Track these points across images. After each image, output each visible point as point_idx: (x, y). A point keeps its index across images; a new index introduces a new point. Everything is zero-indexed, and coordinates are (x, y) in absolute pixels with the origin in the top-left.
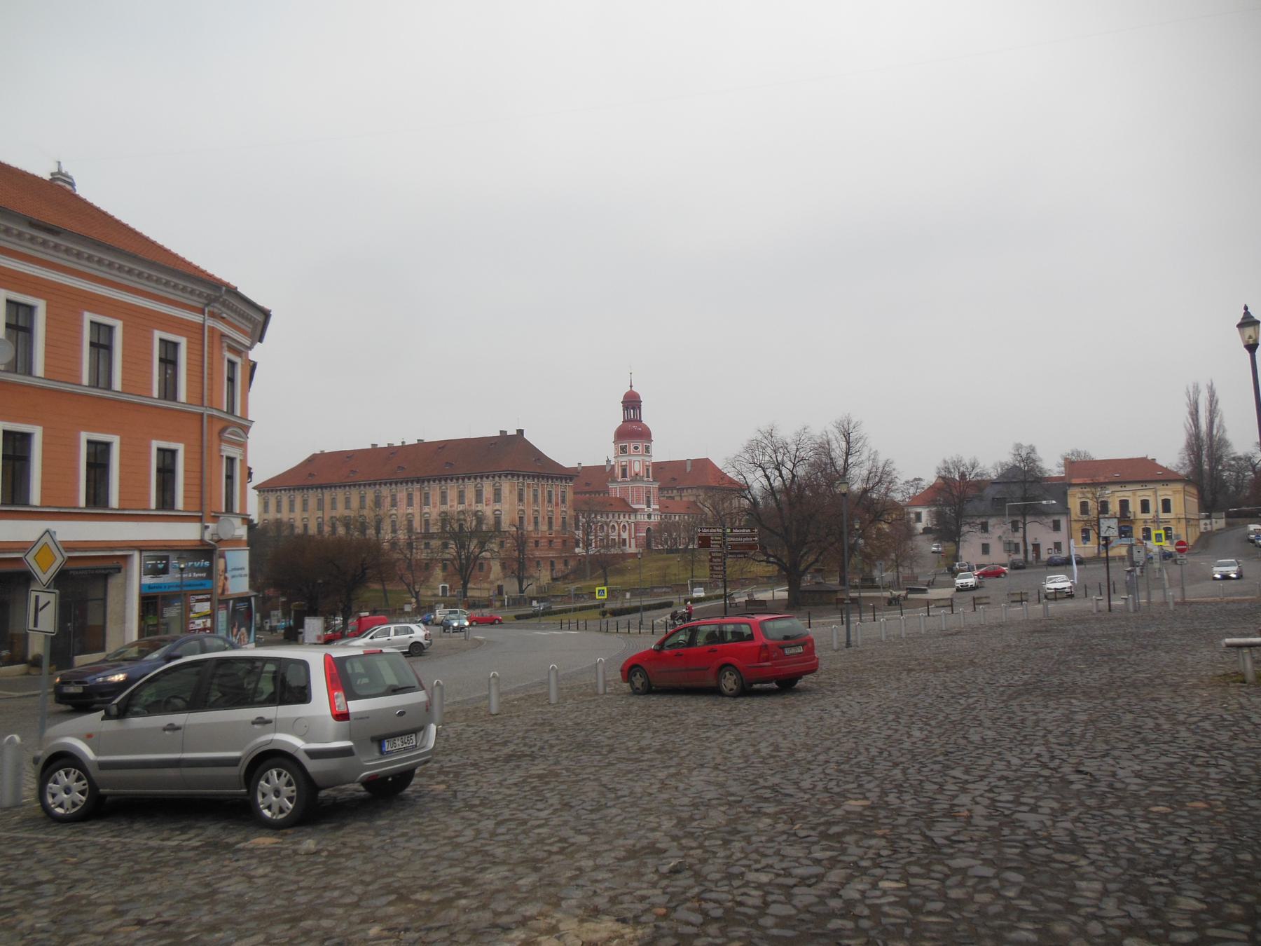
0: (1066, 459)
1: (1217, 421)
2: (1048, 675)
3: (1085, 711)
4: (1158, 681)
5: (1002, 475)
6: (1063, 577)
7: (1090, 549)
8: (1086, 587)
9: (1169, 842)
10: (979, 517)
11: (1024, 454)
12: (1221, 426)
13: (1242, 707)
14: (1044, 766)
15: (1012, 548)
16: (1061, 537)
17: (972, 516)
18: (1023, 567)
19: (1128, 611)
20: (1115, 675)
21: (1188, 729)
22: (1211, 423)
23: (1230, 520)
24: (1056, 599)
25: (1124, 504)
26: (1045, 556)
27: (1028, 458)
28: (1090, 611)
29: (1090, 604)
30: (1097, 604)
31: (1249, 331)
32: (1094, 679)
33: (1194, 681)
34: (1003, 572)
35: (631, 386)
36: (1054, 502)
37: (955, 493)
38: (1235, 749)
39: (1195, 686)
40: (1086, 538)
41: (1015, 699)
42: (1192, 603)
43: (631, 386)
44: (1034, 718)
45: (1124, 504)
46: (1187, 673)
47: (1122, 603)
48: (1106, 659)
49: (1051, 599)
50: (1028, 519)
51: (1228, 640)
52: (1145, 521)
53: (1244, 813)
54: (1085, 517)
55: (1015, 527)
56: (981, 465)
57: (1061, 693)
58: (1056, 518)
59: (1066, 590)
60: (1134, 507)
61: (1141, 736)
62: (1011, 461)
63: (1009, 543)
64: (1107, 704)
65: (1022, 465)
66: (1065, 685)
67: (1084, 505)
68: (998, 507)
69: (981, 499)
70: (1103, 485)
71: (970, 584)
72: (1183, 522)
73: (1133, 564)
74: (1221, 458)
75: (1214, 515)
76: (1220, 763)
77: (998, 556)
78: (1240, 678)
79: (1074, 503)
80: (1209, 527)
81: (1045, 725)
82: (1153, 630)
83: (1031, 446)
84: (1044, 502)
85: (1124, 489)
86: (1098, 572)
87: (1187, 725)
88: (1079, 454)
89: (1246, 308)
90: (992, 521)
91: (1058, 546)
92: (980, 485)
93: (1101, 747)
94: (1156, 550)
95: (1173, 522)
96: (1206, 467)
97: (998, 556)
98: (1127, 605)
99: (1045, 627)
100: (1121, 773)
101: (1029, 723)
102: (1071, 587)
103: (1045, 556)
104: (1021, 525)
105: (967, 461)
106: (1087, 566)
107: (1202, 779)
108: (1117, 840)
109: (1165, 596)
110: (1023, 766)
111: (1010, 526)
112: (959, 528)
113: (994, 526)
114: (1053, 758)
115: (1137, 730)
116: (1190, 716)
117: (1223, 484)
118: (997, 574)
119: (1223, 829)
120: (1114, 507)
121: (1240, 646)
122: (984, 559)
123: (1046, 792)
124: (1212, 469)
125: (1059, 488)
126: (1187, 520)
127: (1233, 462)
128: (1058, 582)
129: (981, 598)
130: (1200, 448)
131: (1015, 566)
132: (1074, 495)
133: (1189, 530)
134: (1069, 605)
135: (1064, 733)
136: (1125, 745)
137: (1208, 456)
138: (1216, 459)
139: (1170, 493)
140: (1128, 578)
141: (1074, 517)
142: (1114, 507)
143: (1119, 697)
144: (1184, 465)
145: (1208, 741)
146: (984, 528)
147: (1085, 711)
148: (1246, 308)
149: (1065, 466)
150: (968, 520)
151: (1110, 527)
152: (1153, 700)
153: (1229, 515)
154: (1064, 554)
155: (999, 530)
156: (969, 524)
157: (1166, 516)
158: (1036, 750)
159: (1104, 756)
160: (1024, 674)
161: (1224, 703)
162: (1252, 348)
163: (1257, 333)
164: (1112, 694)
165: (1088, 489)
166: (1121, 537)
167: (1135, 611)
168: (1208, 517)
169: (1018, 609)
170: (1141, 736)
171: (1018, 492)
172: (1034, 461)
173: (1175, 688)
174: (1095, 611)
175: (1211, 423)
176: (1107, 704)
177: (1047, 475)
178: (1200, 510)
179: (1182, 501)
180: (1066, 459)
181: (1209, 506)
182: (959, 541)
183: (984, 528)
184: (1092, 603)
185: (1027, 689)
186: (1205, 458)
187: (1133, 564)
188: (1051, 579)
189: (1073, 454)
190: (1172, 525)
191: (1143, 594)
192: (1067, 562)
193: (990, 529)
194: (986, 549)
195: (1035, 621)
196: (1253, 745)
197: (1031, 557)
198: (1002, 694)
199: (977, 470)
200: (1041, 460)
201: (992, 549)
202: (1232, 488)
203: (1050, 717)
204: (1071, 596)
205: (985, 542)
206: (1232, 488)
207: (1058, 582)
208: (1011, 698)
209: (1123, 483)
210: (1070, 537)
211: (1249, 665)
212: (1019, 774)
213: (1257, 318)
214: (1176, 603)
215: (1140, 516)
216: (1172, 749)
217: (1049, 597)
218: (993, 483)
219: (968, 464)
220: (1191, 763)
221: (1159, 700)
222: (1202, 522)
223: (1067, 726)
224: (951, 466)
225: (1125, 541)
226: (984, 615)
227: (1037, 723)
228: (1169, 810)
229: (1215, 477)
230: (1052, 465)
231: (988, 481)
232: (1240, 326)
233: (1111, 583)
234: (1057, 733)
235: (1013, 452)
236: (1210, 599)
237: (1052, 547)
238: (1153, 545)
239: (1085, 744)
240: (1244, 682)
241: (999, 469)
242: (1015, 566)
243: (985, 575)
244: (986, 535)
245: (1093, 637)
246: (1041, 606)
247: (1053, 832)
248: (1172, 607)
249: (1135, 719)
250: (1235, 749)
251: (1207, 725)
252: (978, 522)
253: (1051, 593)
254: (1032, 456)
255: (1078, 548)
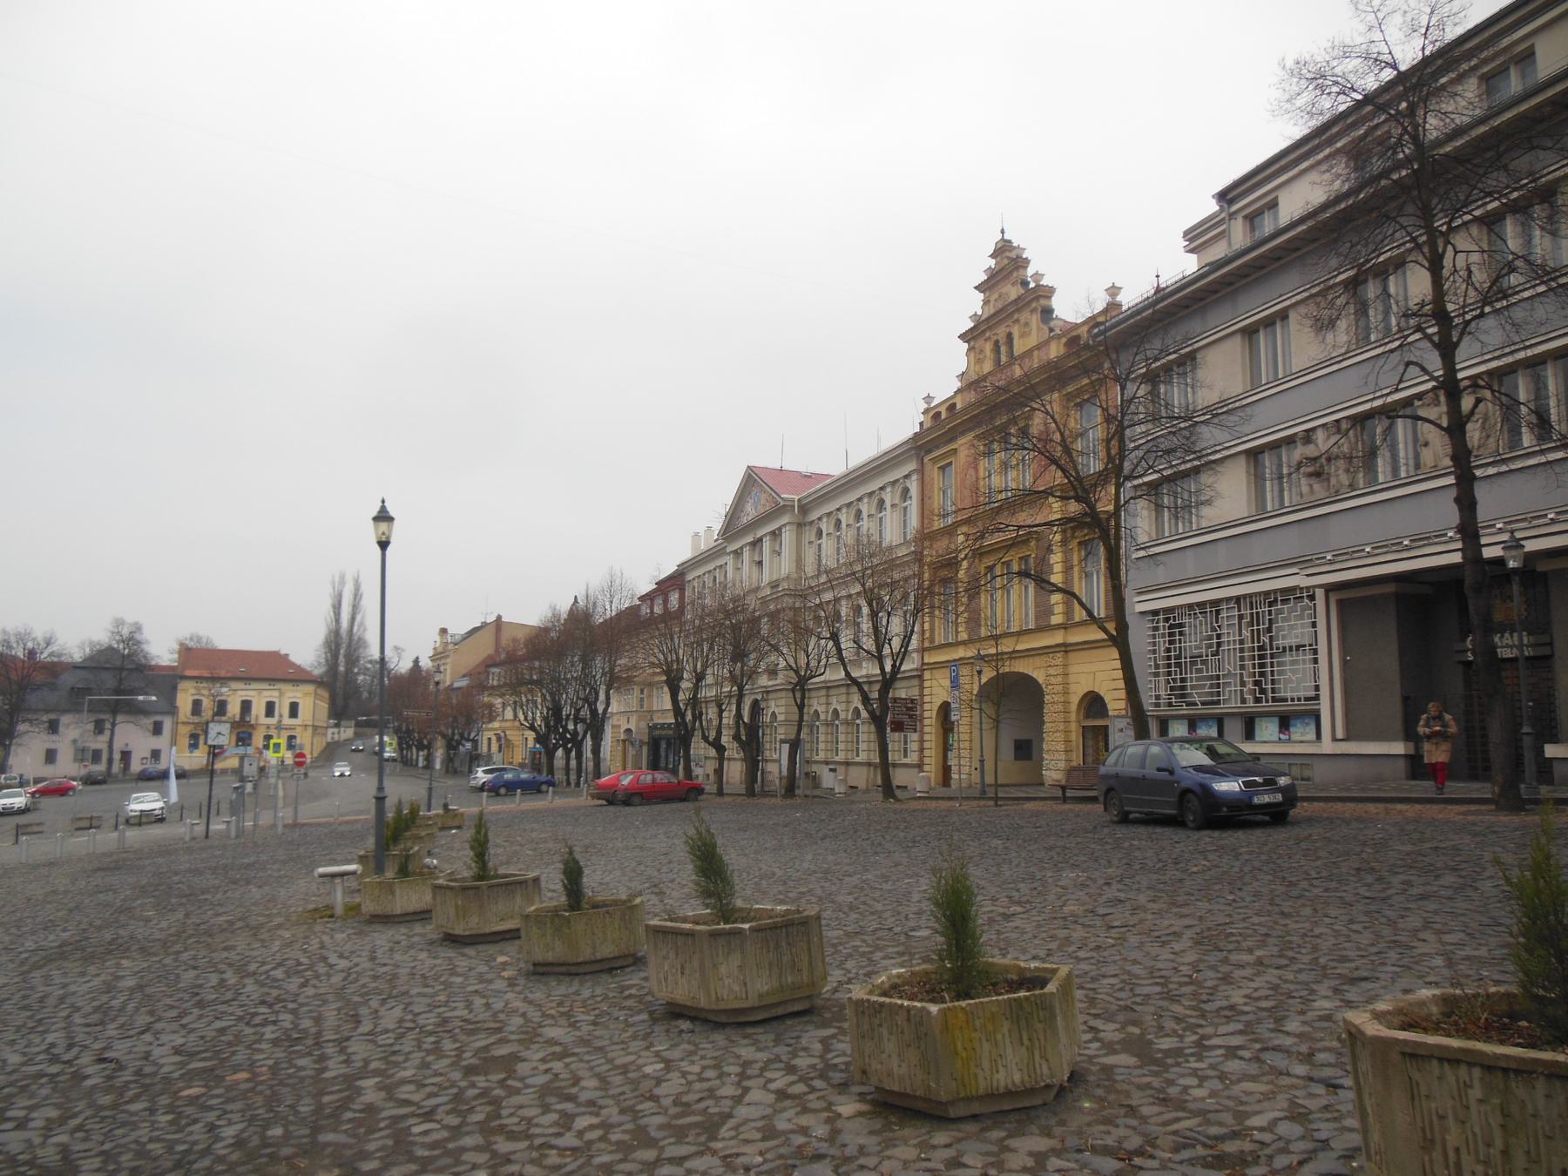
0: (182, 644)
1: (358, 618)
2: (99, 928)
3: (136, 974)
4: (240, 924)
5: (91, 658)
6: (155, 795)
7: (199, 758)
8: (182, 808)
9: (191, 1133)
10: (47, 711)
11: (125, 632)
12: (362, 624)
13: (322, 947)
14: (55, 1059)
15: (81, 754)
16: (161, 742)
17: (36, 711)
18: (102, 782)
19: (228, 837)
20: (189, 922)
21: (257, 982)
22: (353, 619)
23: (360, 730)
24: (140, 824)
25: (246, 706)
26: (136, 766)
27: (131, 639)
28: (182, 839)
29: (183, 830)
30: (192, 830)
31: (383, 526)
32: (161, 930)
33: (279, 920)
34: (72, 788)
35: (1003, 232)
36: (154, 698)
37: (13, 676)
38: (301, 1000)
39: (279, 926)
40: (194, 746)
41: (40, 967)
42: (304, 825)
43: (1003, 232)
44: (61, 992)
45: (246, 706)
46: (275, 911)
47: (223, 827)
48: (184, 900)
49: (134, 825)
50: (120, 718)
51: (321, 870)
52: (268, 727)
53: (290, 1076)
54: (196, 719)
55: (99, 728)
56: (61, 641)
57: (110, 952)
58: (158, 718)
59: (157, 812)
60: (258, 709)
61: (198, 998)
62: (107, 640)
63: (83, 750)
64: (168, 961)
65: (121, 646)
66: (120, 941)
67: (197, 705)
68: (77, 699)
69: (53, 687)
70: (224, 680)
71: (17, 806)
72: (310, 730)
73: (243, 779)
74: (358, 659)
75: (343, 723)
76: (281, 1018)
77: (67, 768)
78: (329, 913)
79: (184, 701)
80: (336, 737)
81: (73, 1000)
82: (252, 859)
83: (136, 623)
84: (141, 698)
85: (248, 687)
86: (199, 787)
87: (257, 977)
88: (199, 639)
89: (383, 502)
90: (65, 719)
91: (156, 754)
92: (55, 669)
93: (142, 1020)
94: (274, 762)
95: (299, 730)
96: (342, 669)
97: (67, 768)
98: (228, 830)
99: (114, 864)
100: (157, 1052)
101: (51, 1001)
102: (162, 808)
103: (136, 766)
104: (108, 725)
105: (39, 633)
106: (191, 781)
107: (255, 1042)
108: (125, 1145)
109: (275, 816)
110: (24, 1064)
111: (91, 727)
112: (12, 725)
113: (69, 725)
114: (70, 1047)
115: (196, 990)
116: (263, 963)
117: (357, 689)
118: (62, 791)
119: (259, 1100)
120: (234, 709)
121: (333, 876)
122: (48, 771)
123: (47, 1098)
124: (348, 671)
125: (166, 681)
126: (315, 728)
127: (369, 666)
128: (146, 801)
129: (30, 825)
130: (338, 646)
131: (90, 781)
132: (185, 690)
133: (315, 740)
134: (156, 831)
135: (97, 1009)
136: (174, 1013)
137: (345, 656)
138: (352, 660)
139: (299, 695)
140: (234, 796)
141: (182, 718)
142: (234, 709)
143: (186, 950)
144: (320, 663)
145: (275, 993)
146: (53, 727)
147: (136, 974)
148: (383, 502)
149: (180, 652)
150: (29, 716)
151: (220, 733)
152: (226, 949)
153: (358, 725)
154: (162, 766)
155: (74, 730)
156: (30, 721)
157: (293, 721)
158: (50, 1038)
159: (143, 1033)
160: (65, 930)
161: (305, 944)
162: (384, 545)
163: (390, 530)
164: (178, 947)
165: (205, 685)
166: (237, 745)
167: (237, 837)
168: (337, 725)
169: (82, 839)
170: (198, 998)
171: (110, 681)
172: (138, 643)
173: (255, 931)
174: (187, 839)
175: (353, 619)
176: (168, 961)
177: (153, 663)
178: (330, 717)
179: (312, 705)
180: (182, 644)
181: (339, 713)
182: (10, 745)
183: (53, 727)
184: (191, 826)
185: (62, 953)
186: (341, 659)
187: (243, 779)
188: (137, 798)
189: (191, 639)
190: (298, 733)
191: (249, 816)
192: (164, 775)
193: (61, 729)
194: (51, 756)
195: (104, 854)
196: (322, 991)
197: (116, 768)
198: (22, 963)
199: (54, 648)
200: (147, 642)
201: (59, 757)
202: (365, 695)
203: (85, 987)
204: (161, 820)
205: (52, 746)
206: (365, 695)
207: (146, 801)
208: (36, 967)
209: (248, 679)
210: (173, 742)
211: (339, 895)
212: (15, 1077)
213: (392, 513)
214: (285, 826)
215: (264, 720)
216: (230, 1010)
217: (132, 821)
218: (76, 667)
219: (40, 639)
220: (247, 1024)
221: (233, 948)
222: (330, 731)
223: (104, 998)
224: (13, 639)
225: (241, 750)
226: (34, 849)
227: (62, 999)
228: (203, 1090)
229: (349, 677)
230: (161, 650)
231: (68, 664)
232: (376, 519)
233: (214, 801)
234: (88, 1009)
235: (111, 628)
236: (323, 820)
237: (148, 755)
238: (271, 756)
239: (121, 1020)
240: (332, 916)
241: (87, 650)
242: (90, 781)
243: (45, 792)
244: (54, 737)
245: (176, 873)
246: (115, 834)
247: (40, 1152)
248: (280, 829)
249: (197, 977)
250: (301, 1000)
251: (279, 973)
252: (45, 718)
253: (135, 817)
254: (137, 636)
255: (179, 757)
